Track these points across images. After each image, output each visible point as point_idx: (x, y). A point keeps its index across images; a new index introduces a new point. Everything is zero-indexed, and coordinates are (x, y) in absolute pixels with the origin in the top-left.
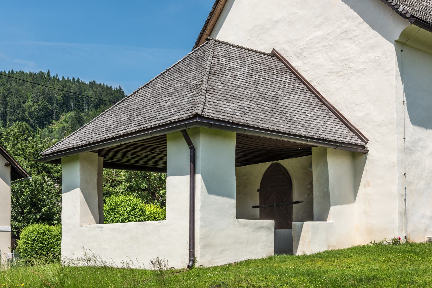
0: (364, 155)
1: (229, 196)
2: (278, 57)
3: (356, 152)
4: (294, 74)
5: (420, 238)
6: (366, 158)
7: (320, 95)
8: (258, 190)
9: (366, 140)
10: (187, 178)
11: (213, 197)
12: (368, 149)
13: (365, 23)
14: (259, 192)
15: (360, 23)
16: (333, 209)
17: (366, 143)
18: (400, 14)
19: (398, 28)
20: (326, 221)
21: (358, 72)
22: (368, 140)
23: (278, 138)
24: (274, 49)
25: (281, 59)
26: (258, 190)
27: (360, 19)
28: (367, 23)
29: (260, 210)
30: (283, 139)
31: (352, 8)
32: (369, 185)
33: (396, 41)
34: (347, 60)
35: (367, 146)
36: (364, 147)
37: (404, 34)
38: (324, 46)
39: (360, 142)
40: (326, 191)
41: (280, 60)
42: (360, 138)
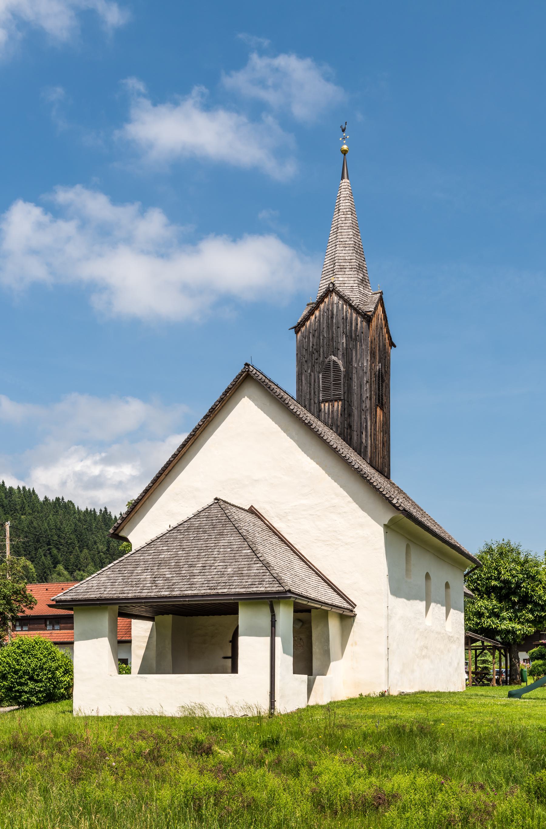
0: (352, 619)
1: (291, 656)
2: (256, 515)
3: (347, 617)
4: (276, 534)
5: (394, 692)
6: (354, 621)
7: (305, 558)
8: (230, 642)
9: (354, 605)
10: (268, 639)
11: (285, 655)
12: (356, 613)
13: (354, 503)
14: (231, 644)
15: (349, 502)
16: (332, 664)
17: (354, 608)
18: (394, 505)
19: (387, 516)
20: (325, 675)
21: (346, 544)
22: (356, 605)
23: (305, 603)
24: (252, 506)
25: (259, 516)
26: (230, 642)
27: (350, 499)
28: (357, 504)
29: (232, 661)
30: (309, 604)
31: (341, 487)
32: (356, 644)
33: (384, 525)
34: (336, 531)
35: (354, 610)
36: (352, 611)
37: (391, 521)
38: (311, 515)
39: (346, 605)
40: (326, 649)
41: (259, 518)
42: (348, 602)
